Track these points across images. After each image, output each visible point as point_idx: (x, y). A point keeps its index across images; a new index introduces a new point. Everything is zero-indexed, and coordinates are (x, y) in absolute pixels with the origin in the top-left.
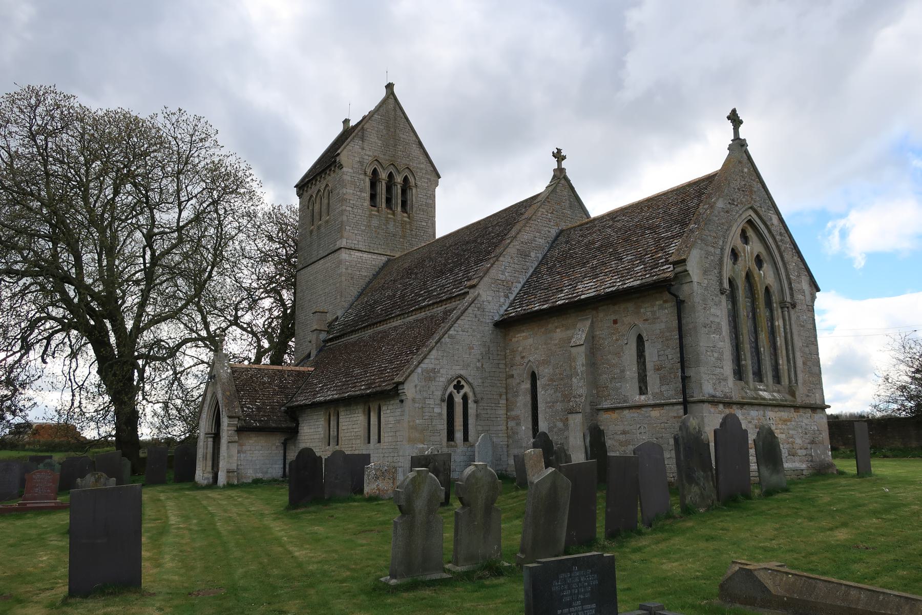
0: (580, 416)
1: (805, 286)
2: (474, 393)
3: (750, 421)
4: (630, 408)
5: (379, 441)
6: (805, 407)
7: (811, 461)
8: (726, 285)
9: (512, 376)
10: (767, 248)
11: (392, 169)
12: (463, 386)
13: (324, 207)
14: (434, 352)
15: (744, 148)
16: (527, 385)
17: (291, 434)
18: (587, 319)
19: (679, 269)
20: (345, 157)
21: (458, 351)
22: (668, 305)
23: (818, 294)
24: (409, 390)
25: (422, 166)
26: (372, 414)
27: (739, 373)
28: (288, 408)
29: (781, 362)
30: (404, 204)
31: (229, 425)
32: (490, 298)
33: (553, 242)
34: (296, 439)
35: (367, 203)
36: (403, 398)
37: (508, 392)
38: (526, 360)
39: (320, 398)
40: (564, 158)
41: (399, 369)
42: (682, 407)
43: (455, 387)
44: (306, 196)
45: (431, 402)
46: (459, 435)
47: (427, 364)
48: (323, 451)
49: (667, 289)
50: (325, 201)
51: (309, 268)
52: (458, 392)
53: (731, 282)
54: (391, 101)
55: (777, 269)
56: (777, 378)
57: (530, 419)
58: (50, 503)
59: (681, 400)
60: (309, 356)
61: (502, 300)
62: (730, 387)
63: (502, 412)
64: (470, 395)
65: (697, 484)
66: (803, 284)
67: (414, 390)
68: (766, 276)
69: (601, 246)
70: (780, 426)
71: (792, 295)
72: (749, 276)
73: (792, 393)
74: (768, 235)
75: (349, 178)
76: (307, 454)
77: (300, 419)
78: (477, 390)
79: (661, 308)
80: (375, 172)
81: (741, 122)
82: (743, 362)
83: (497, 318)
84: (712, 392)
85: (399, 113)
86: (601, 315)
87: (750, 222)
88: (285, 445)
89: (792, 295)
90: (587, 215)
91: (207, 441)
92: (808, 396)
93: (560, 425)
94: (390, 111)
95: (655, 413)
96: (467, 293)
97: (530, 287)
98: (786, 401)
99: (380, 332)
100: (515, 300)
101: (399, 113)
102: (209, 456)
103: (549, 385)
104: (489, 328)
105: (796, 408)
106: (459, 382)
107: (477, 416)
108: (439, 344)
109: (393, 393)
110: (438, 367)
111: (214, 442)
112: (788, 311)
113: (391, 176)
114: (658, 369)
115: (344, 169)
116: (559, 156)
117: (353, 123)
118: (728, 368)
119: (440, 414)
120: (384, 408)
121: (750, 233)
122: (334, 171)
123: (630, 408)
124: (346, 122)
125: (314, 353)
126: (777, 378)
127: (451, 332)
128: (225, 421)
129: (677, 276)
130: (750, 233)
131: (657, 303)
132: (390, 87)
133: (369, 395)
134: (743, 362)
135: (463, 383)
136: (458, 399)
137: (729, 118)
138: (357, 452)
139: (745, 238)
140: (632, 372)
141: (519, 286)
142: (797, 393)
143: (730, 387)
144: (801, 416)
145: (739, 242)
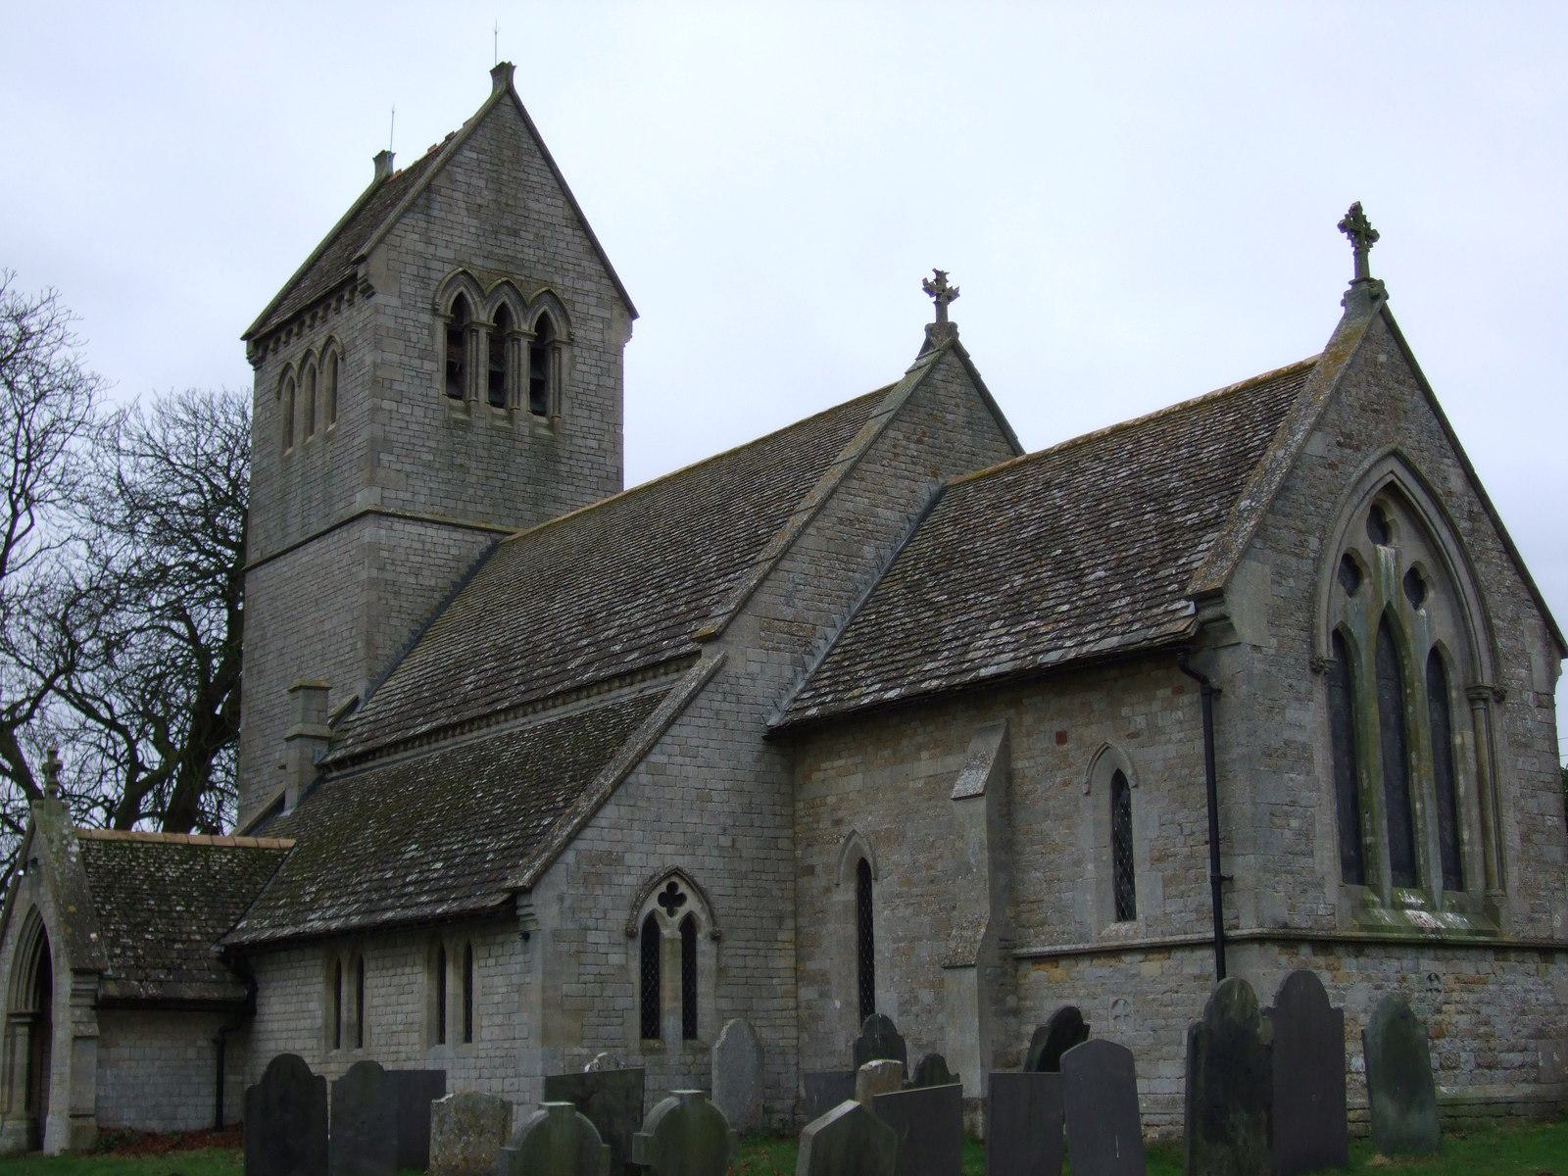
0: (972, 974)
1: (1536, 651)
2: (712, 915)
3: (1355, 991)
5: (468, 1038)
6: (1523, 949)
8: (1325, 649)
9: (810, 870)
11: (506, 297)
12: (682, 899)
13: (322, 400)
14: (610, 812)
15: (1377, 305)
16: (847, 894)
17: (235, 1020)
18: (994, 729)
19: (1208, 613)
21: (677, 801)
22: (1185, 699)
24: (545, 911)
27: (1356, 866)
28: (229, 948)
29: (1466, 835)
30: (538, 390)
31: (75, 994)
32: (754, 668)
33: (924, 517)
35: (439, 385)
36: (532, 927)
38: (846, 830)
39: (315, 923)
40: (952, 295)
41: (512, 856)
43: (663, 899)
44: (273, 368)
46: (671, 1022)
47: (592, 841)
48: (331, 1066)
49: (1184, 660)
50: (324, 382)
51: (280, 563)
52: (671, 913)
53: (1340, 638)
55: (1460, 605)
56: (1455, 875)
57: (854, 981)
59: (1211, 935)
60: (280, 804)
61: (788, 673)
62: (1326, 903)
63: (784, 962)
64: (702, 917)
67: (555, 909)
68: (1430, 623)
69: (1038, 537)
70: (1456, 996)
72: (1389, 626)
73: (1490, 910)
75: (391, 323)
76: (289, 1067)
78: (722, 906)
80: (460, 304)
81: (1372, 236)
82: (1369, 840)
83: (774, 720)
84: (1283, 914)
85: (527, 143)
86: (1028, 719)
87: (1392, 490)
88: (220, 1047)
90: (1016, 449)
91: (14, 1036)
92: (1531, 920)
93: (926, 996)
94: (503, 128)
95: (1152, 967)
96: (697, 654)
97: (864, 639)
100: (818, 672)
101: (527, 143)
102: (20, 1073)
103: (899, 895)
104: (748, 749)
105: (1501, 950)
106: (672, 887)
107: (721, 971)
108: (621, 791)
111: (32, 1036)
112: (1487, 710)
113: (502, 315)
114: (1159, 859)
115: (379, 299)
116: (940, 291)
117: (401, 164)
118: (1326, 857)
119: (623, 968)
120: (479, 953)
121: (1394, 515)
122: (351, 303)
124: (383, 159)
125: (292, 798)
126: (1455, 875)
128: (63, 983)
129: (1203, 628)
130: (1394, 515)
132: (503, 73)
133: (442, 919)
134: (1369, 840)
135: (683, 888)
136: (670, 929)
137: (1343, 227)
138: (410, 1066)
139: (1380, 530)
140: (1097, 869)
141: (832, 635)
142: (1503, 913)
145: (1362, 541)
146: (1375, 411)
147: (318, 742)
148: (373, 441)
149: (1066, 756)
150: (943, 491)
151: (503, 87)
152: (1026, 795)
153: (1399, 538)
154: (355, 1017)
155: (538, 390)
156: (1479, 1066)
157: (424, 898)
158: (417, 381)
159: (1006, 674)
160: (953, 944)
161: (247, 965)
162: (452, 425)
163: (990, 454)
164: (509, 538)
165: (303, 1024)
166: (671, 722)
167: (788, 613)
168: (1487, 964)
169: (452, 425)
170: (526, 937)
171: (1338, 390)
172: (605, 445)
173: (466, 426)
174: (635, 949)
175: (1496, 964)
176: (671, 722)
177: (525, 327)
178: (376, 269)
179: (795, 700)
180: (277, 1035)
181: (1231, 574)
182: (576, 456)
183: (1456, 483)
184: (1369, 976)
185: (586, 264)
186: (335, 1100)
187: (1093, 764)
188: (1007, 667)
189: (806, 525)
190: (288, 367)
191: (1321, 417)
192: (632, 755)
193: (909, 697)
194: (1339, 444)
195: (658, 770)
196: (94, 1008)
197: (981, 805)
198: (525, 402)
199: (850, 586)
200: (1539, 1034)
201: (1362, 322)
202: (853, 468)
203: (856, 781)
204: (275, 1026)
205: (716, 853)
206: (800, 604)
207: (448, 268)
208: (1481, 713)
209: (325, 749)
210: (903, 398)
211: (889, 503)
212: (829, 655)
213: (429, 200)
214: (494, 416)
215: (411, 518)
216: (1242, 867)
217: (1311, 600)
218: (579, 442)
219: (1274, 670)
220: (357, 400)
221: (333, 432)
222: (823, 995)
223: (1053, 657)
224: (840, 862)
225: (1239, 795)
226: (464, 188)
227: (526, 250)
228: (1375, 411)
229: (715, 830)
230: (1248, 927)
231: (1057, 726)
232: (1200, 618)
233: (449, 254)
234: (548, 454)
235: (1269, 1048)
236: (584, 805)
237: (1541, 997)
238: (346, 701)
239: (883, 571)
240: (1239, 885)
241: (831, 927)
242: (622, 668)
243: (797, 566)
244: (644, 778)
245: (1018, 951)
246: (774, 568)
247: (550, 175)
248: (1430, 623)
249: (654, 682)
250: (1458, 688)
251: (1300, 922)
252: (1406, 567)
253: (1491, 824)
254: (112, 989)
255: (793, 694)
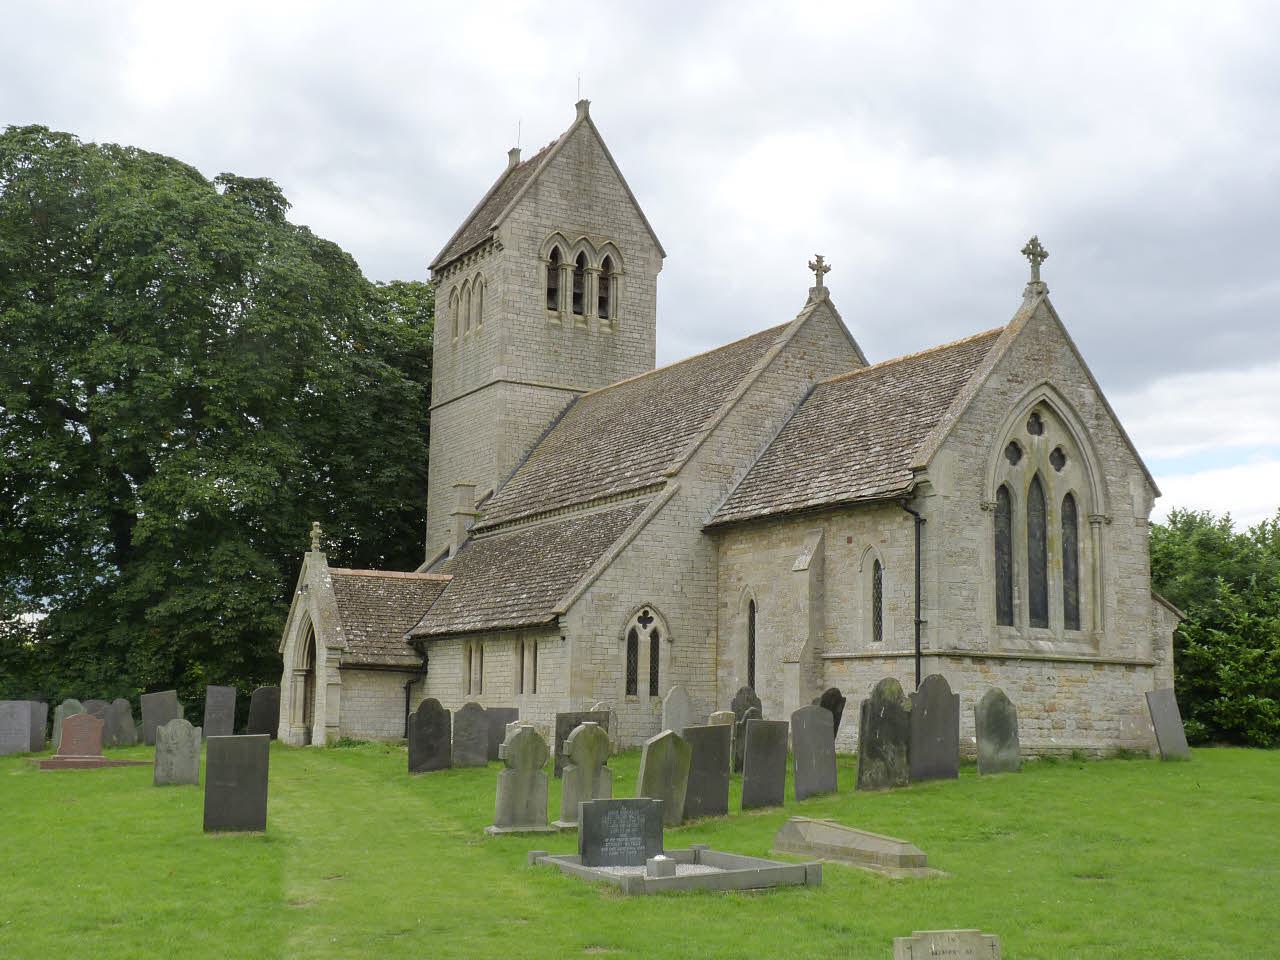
1: (1136, 491)
4: (862, 658)
5: (535, 692)
7: (1117, 737)
8: (991, 497)
9: (725, 605)
10: (1072, 438)
12: (651, 619)
17: (417, 675)
19: (919, 478)
20: (513, 229)
21: (651, 564)
23: (1157, 500)
24: (571, 625)
25: (635, 238)
26: (526, 653)
30: (603, 303)
31: (329, 660)
32: (697, 492)
34: (424, 683)
36: (566, 634)
37: (715, 628)
38: (743, 584)
41: (560, 593)
42: (914, 661)
45: (604, 639)
46: (643, 686)
49: (906, 502)
50: (475, 300)
52: (645, 627)
54: (585, 132)
56: (1072, 619)
58: (87, 758)
59: (914, 652)
60: (447, 553)
61: (717, 494)
62: (984, 633)
63: (709, 655)
64: (662, 631)
65: (883, 759)
66: (1132, 487)
71: (1108, 504)
72: (1037, 480)
73: (1095, 643)
74: (1073, 420)
77: (429, 653)
78: (673, 624)
79: (902, 527)
83: (708, 521)
84: (954, 642)
86: (834, 529)
88: (408, 689)
89: (1108, 504)
90: (864, 362)
92: (1122, 648)
94: (583, 147)
98: (1084, 655)
99: (549, 527)
101: (598, 150)
105: (1098, 664)
106: (646, 613)
107: (673, 659)
109: (552, 627)
110: (616, 592)
115: (505, 252)
117: (525, 157)
118: (987, 608)
119: (617, 657)
122: (490, 253)
123: (862, 658)
124: (514, 153)
125: (454, 549)
126: (1072, 619)
127: (635, 543)
128: (322, 654)
129: (916, 487)
130: (1046, 418)
131: (897, 519)
132: (583, 106)
133: (521, 627)
135: (651, 614)
136: (644, 637)
141: (744, 472)
143: (984, 633)
144: (1105, 675)
146: (1035, 360)
147: (468, 517)
148: (503, 338)
149: (851, 550)
150: (815, 387)
151: (582, 115)
152: (831, 570)
153: (1049, 431)
154: (478, 676)
155: (603, 303)
156: (1079, 728)
157: (514, 615)
158: (528, 301)
159: (822, 504)
160: (789, 650)
161: (421, 645)
162: (550, 327)
163: (847, 364)
164: (584, 395)
165: (452, 680)
166: (648, 522)
167: (718, 460)
168: (1089, 672)
169: (550, 327)
170: (564, 638)
171: (1010, 349)
172: (645, 337)
173: (560, 328)
174: (624, 646)
175: (1094, 672)
176: (648, 522)
177: (595, 266)
178: (504, 235)
179: (720, 510)
180: (439, 686)
181: (932, 457)
182: (627, 343)
183: (1089, 396)
184: (1008, 677)
185: (634, 224)
186: (455, 722)
187: (864, 556)
188: (822, 501)
189: (730, 409)
190: (455, 288)
191: (996, 366)
192: (625, 540)
193: (774, 513)
194: (1009, 380)
195: (636, 549)
196: (339, 668)
197: (806, 575)
198: (595, 311)
199: (755, 444)
200: (1121, 712)
201: (1030, 309)
202: (761, 375)
203: (748, 557)
204: (437, 681)
205: (671, 594)
206: (725, 455)
207: (548, 231)
208: (1096, 531)
209: (472, 521)
210: (795, 329)
211: (779, 397)
212: (741, 484)
213: (537, 189)
214: (576, 321)
215: (525, 384)
216: (929, 615)
217: (983, 470)
218: (628, 335)
219: (957, 509)
220: (494, 313)
221: (481, 330)
222: (730, 674)
223: (843, 496)
224: (739, 602)
225: (930, 577)
226: (558, 180)
227: (597, 218)
228: (1035, 360)
229: (672, 582)
230: (934, 649)
231: (849, 533)
232: (915, 480)
233: (548, 223)
234: (610, 345)
235: (909, 714)
236: (598, 567)
237: (1125, 691)
238: (487, 492)
239: (777, 434)
240: (929, 626)
241: (735, 636)
242: (628, 488)
243: (724, 434)
244: (630, 554)
245: (825, 655)
246: (710, 435)
247: (611, 170)
248: (1064, 481)
249: (644, 497)
250: (1083, 516)
251: (965, 646)
252: (1052, 448)
253: (1098, 593)
254: (350, 659)
255: (720, 507)
